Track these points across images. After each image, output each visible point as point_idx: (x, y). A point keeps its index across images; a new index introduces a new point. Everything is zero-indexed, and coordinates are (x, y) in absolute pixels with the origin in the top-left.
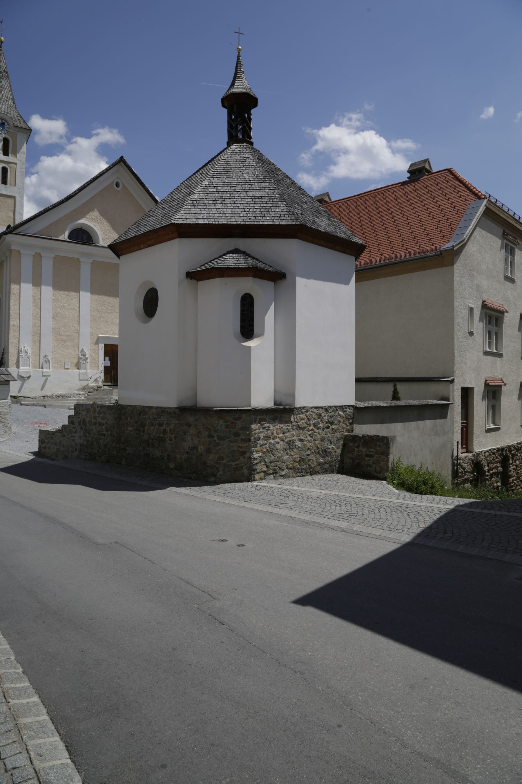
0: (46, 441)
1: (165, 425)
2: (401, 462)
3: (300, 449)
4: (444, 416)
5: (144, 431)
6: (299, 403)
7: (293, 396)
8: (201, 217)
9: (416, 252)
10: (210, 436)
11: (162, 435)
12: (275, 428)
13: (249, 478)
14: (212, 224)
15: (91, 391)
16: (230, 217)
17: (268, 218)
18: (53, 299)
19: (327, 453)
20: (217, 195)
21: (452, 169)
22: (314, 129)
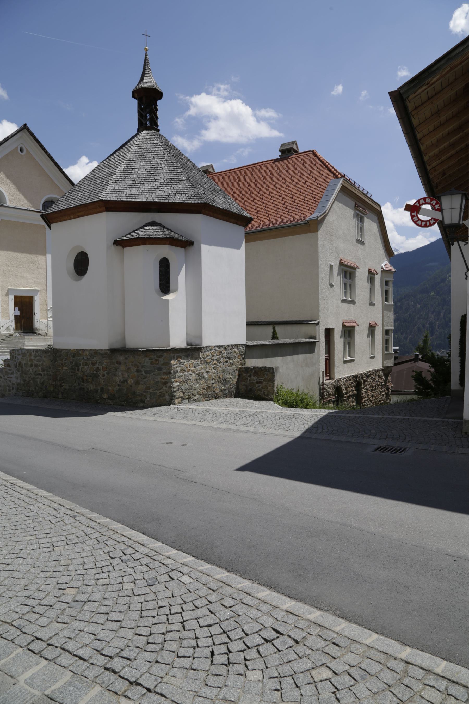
1: (97, 364)
2: (283, 387)
3: (207, 379)
4: (312, 351)
5: (78, 370)
7: (201, 337)
8: (124, 195)
9: (289, 220)
10: (138, 371)
11: (95, 372)
12: (188, 363)
13: (170, 403)
14: (134, 201)
15: (3, 338)
16: (148, 196)
17: (178, 197)
19: (227, 381)
20: (135, 176)
21: (315, 151)
22: (187, 96)
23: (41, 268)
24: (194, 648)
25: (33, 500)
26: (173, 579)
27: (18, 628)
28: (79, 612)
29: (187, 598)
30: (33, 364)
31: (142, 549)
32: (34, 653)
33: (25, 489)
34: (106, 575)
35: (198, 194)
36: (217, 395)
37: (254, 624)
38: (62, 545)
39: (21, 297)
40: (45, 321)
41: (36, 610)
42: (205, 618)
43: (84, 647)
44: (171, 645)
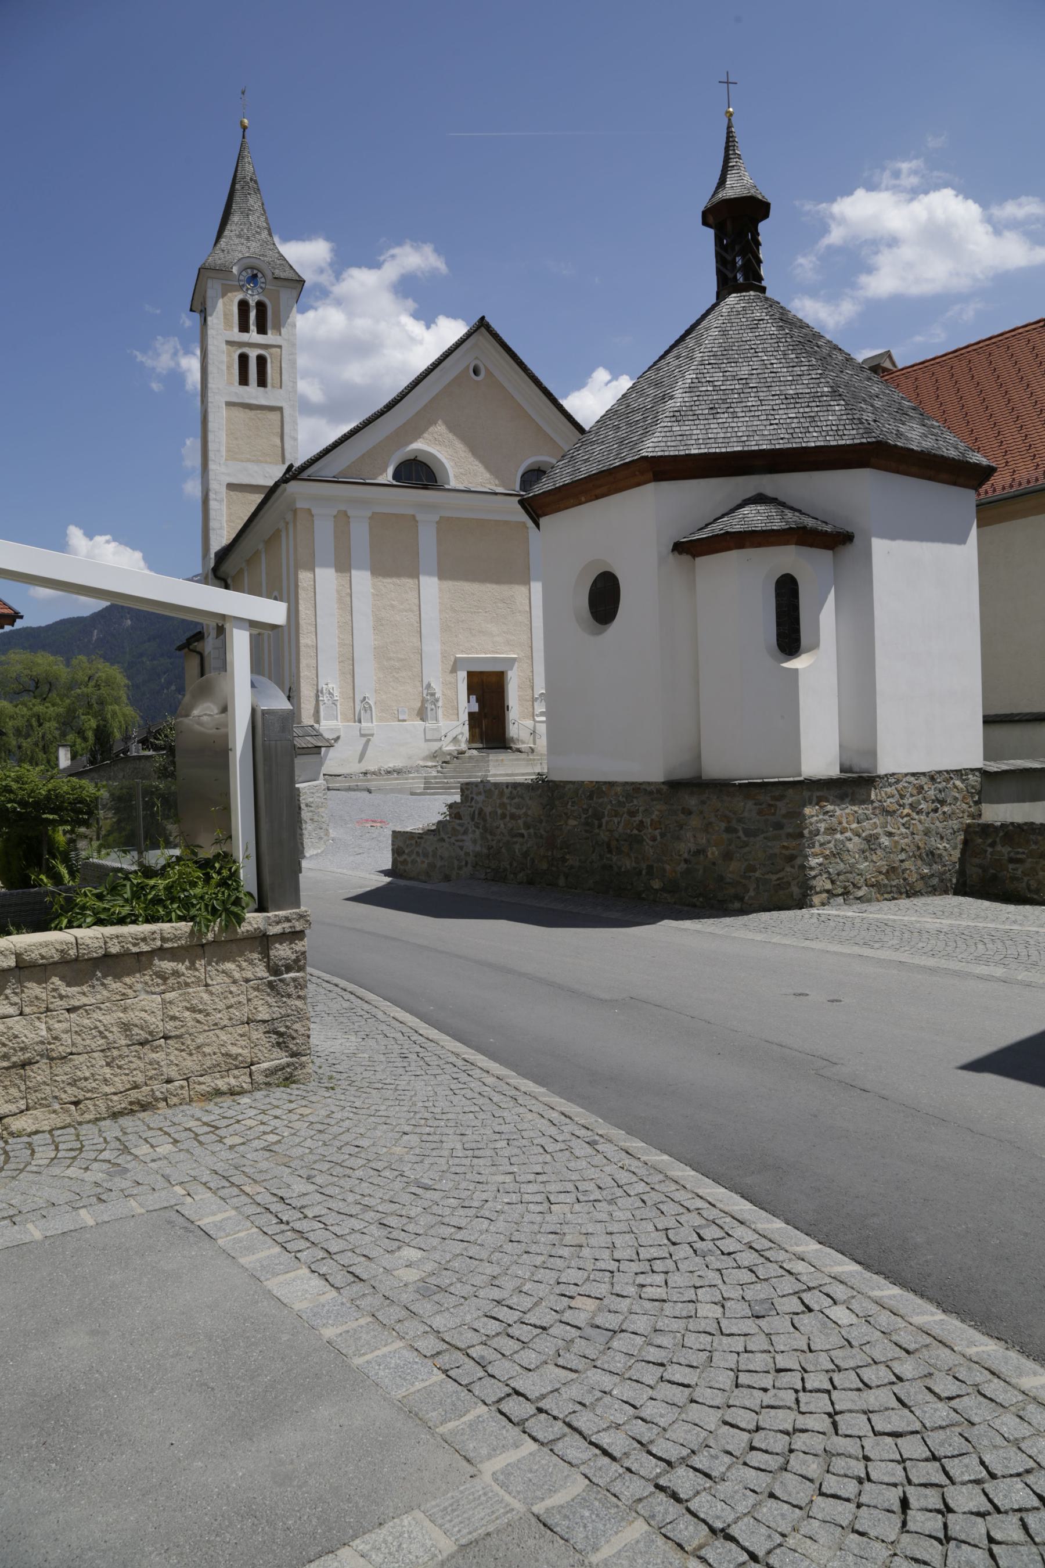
0: (406, 851)
5: (600, 826)
6: (885, 766)
7: (873, 754)
8: (693, 442)
10: (729, 830)
11: (635, 832)
12: (843, 812)
13: (802, 903)
16: (745, 438)
17: (815, 434)
18: (373, 595)
22: (822, 202)
23: (520, 612)
24: (860, 1481)
25: (509, 1099)
26: (810, 1310)
27: (479, 1364)
28: (603, 1353)
29: (844, 1359)
30: (508, 813)
31: (740, 1231)
32: (510, 1421)
33: (493, 1075)
34: (659, 1279)
35: (862, 423)
36: (911, 888)
37: (1012, 1454)
38: (568, 1201)
39: (482, 673)
40: (529, 723)
41: (515, 1331)
42: (886, 1413)
43: (612, 1430)
44: (804, 1462)
